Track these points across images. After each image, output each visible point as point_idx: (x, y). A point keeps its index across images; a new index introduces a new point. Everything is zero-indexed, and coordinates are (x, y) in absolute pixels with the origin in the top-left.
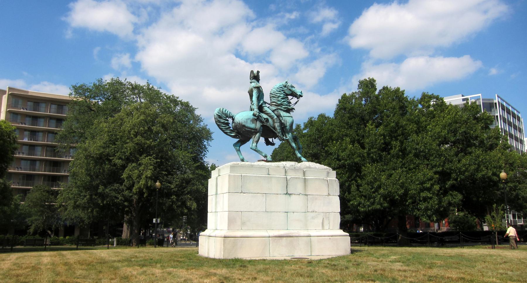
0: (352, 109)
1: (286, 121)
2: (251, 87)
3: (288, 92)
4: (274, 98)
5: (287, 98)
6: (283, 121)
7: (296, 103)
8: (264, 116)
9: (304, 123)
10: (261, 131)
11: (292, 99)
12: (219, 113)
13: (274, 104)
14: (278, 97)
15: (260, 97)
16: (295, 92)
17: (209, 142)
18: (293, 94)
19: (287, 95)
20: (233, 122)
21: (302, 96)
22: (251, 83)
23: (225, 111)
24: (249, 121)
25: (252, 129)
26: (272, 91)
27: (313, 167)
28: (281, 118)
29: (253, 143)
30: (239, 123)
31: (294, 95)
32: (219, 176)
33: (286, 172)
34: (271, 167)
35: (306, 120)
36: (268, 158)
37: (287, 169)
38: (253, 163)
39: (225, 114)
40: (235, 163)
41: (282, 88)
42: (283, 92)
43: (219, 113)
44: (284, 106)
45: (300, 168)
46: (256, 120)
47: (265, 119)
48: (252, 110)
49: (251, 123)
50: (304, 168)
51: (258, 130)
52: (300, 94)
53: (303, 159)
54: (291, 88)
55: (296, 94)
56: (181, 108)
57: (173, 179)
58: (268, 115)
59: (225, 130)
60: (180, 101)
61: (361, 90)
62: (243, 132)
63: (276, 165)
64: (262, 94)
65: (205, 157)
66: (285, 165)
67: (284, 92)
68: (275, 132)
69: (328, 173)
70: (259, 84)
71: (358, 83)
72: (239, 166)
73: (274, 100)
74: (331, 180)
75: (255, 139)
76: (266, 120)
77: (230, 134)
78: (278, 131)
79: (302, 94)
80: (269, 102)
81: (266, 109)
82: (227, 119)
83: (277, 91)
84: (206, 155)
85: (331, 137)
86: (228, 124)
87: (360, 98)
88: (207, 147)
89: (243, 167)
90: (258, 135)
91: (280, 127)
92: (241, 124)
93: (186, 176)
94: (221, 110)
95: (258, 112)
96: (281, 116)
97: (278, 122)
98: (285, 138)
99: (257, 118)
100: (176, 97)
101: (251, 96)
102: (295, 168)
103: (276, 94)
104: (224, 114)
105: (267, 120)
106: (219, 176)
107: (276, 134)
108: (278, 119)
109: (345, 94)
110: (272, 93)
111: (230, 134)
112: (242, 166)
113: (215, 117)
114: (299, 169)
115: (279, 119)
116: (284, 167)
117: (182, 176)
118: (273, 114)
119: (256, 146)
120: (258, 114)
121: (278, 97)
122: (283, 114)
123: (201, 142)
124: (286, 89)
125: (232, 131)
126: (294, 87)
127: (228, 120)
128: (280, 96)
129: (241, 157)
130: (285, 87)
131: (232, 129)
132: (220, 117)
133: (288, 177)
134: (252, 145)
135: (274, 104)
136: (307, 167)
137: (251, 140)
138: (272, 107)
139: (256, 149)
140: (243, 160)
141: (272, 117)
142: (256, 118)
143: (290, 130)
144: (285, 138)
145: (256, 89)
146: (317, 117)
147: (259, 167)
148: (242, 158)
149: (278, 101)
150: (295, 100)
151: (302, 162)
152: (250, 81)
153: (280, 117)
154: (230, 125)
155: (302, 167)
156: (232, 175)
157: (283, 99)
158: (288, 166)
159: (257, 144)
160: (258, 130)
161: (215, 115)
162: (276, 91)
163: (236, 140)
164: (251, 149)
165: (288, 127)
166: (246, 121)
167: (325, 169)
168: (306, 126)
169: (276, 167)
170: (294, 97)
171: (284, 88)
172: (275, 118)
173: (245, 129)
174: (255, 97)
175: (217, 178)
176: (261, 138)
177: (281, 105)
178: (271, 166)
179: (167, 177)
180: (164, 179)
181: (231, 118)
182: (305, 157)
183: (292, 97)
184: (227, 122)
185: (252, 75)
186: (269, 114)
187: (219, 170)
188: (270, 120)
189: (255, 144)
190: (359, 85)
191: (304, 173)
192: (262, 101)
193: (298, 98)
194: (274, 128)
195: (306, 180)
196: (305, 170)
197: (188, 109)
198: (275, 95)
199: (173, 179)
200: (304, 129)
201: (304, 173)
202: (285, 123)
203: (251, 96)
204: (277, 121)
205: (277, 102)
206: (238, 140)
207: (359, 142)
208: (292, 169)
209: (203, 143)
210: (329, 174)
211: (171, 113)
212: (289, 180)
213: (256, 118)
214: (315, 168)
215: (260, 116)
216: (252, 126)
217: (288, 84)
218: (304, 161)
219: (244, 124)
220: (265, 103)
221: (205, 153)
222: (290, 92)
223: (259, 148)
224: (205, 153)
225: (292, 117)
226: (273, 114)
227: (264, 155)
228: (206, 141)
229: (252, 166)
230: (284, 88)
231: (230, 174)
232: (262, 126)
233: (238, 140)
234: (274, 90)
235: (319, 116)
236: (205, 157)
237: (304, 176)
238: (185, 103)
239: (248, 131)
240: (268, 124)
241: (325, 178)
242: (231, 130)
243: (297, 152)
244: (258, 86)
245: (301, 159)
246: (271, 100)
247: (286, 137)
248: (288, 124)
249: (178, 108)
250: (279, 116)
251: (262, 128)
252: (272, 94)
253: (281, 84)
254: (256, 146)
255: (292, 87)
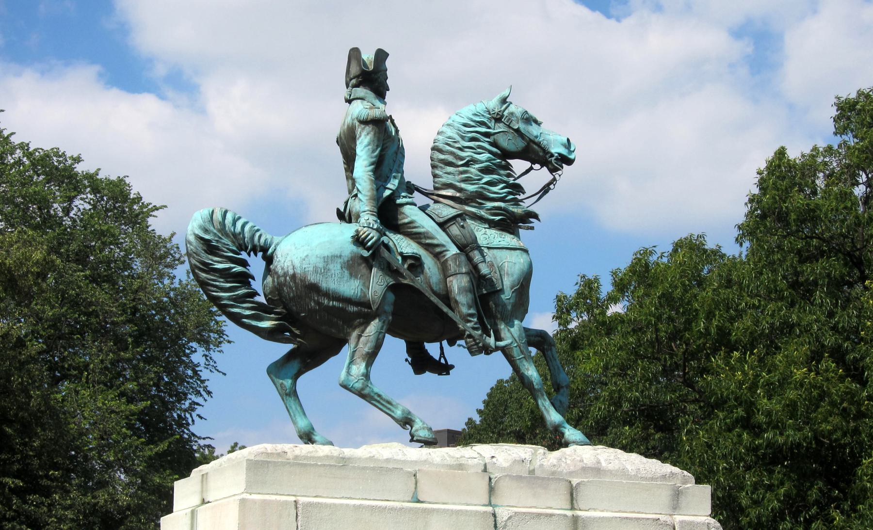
0: (810, 215)
1: (500, 269)
2: (349, 120)
3: (508, 142)
4: (450, 169)
5: (508, 167)
6: (484, 269)
7: (546, 189)
8: (405, 245)
9: (614, 274)
10: (389, 308)
11: (527, 171)
12: (206, 231)
13: (449, 192)
14: (467, 164)
15: (386, 162)
16: (538, 144)
17: (215, 355)
18: (534, 151)
19: (506, 155)
20: (268, 271)
21: (570, 162)
22: (349, 101)
23: (234, 223)
24: (336, 268)
25: (348, 301)
26: (440, 137)
27: (611, 467)
28: (476, 256)
29: (352, 362)
30: (294, 276)
31: (536, 153)
32: (204, 502)
33: (491, 490)
34: (426, 468)
35: (624, 263)
36: (416, 427)
37: (496, 475)
38: (348, 452)
39: (235, 235)
40: (269, 447)
41: (482, 124)
42: (491, 144)
43: (206, 231)
44: (490, 205)
45: (553, 473)
46: (368, 263)
47: (405, 258)
48: (345, 216)
49: (347, 273)
50: (571, 473)
51: (374, 307)
52: (564, 151)
53: (571, 433)
54: (522, 126)
55: (546, 152)
56: (95, 207)
57: (50, 510)
58: (420, 243)
59: (232, 306)
60: (91, 177)
61: (852, 141)
62: (311, 312)
63: (450, 461)
64: (395, 148)
65: (196, 419)
66: (487, 461)
67: (494, 144)
68: (451, 314)
69: (677, 494)
70: (381, 106)
71: (834, 112)
72: (284, 464)
73: (448, 175)
74: (691, 523)
75: (361, 345)
76: (410, 262)
77: (254, 323)
78: (464, 310)
79: (571, 152)
80: (427, 184)
81: (411, 214)
82: (244, 255)
83: (463, 138)
84: (199, 410)
85: (723, 334)
86: (244, 279)
87: (850, 174)
88: (204, 374)
89: (305, 465)
90: (373, 327)
91: (470, 296)
92: (303, 281)
93: (102, 497)
94: (218, 216)
95: (377, 230)
96: (479, 248)
97: (464, 270)
98: (491, 341)
99: (373, 256)
100: (72, 158)
101: (349, 158)
102: (532, 472)
103: (460, 149)
104: (227, 235)
105: (416, 263)
106: (204, 502)
107: (454, 323)
108: (463, 258)
109: (781, 153)
110: (441, 145)
111: (254, 323)
112: (300, 464)
113: (191, 247)
114: (553, 477)
115: (470, 259)
116: (485, 470)
117: (89, 499)
118: (441, 237)
119: (367, 376)
120: (374, 235)
121: (467, 164)
122: (486, 236)
123: (181, 352)
124: (500, 128)
125: (262, 311)
126: (536, 122)
127: (244, 263)
128: (473, 161)
129: (302, 423)
130: (498, 119)
131: (261, 299)
132: (210, 248)
133: (503, 514)
134: (348, 373)
135: (449, 192)
136: (585, 470)
137: (346, 351)
138: (437, 206)
139: (366, 391)
140: (308, 437)
141: (438, 250)
142: (366, 254)
143: (514, 306)
144: (491, 341)
145: (368, 128)
146: (670, 248)
147: (373, 469)
148: (307, 429)
149: (465, 181)
150: (541, 175)
151: (566, 445)
152: (344, 92)
153: (473, 249)
154: (257, 285)
155: (564, 468)
156: (254, 502)
157: (486, 171)
158: (505, 465)
159: (369, 364)
160: (374, 307)
161: (192, 238)
162: (458, 138)
163: (282, 349)
164: (345, 386)
165: (507, 295)
166: (321, 265)
167: (664, 477)
168: (621, 286)
169: (451, 467)
170: (537, 166)
171: (492, 124)
172: (449, 254)
173: (318, 303)
174: (366, 163)
175: (193, 513)
176: (386, 334)
177: (479, 197)
178: (425, 462)
179: (25, 502)
180: (10, 508)
181: (260, 254)
182: (576, 423)
183: (528, 164)
184: (238, 269)
185: (355, 70)
186: (427, 235)
187: (204, 477)
188: (428, 261)
189: (359, 368)
190: (836, 120)
191: (572, 494)
192: (396, 182)
193: (553, 170)
194: (446, 297)
195: (580, 524)
196: (575, 481)
197: (124, 212)
198: (452, 153)
199: (50, 510)
200: (613, 299)
201: (572, 494)
202: (495, 277)
203: (349, 158)
204: (459, 266)
205: (463, 185)
206: (289, 347)
207: (838, 354)
208: (519, 478)
209: (188, 356)
210: (682, 499)
211: (49, 221)
212: (505, 526)
213: (366, 254)
214: (623, 473)
215: (387, 247)
216: (350, 287)
217: (512, 108)
218: (576, 443)
219: (312, 278)
220: (411, 188)
221: (199, 400)
222: (520, 144)
223: (377, 386)
224: (199, 400)
225: (525, 251)
226: (441, 237)
227: (398, 413)
228: (201, 351)
229: (344, 463)
230: (492, 124)
231: (247, 496)
232: (391, 288)
233: (289, 347)
234: (450, 132)
235: (678, 246)
236: (196, 419)
237: (572, 508)
238: (110, 183)
239: (329, 309)
240: (419, 282)
241: (663, 518)
242: (259, 307)
243: (547, 403)
244: (376, 113)
245: (563, 434)
246: (435, 176)
247: (498, 338)
248: (507, 282)
249: (82, 204)
250: (467, 247)
251: (391, 297)
252: (440, 151)
253: (480, 107)
254: (367, 376)
255: (529, 120)
